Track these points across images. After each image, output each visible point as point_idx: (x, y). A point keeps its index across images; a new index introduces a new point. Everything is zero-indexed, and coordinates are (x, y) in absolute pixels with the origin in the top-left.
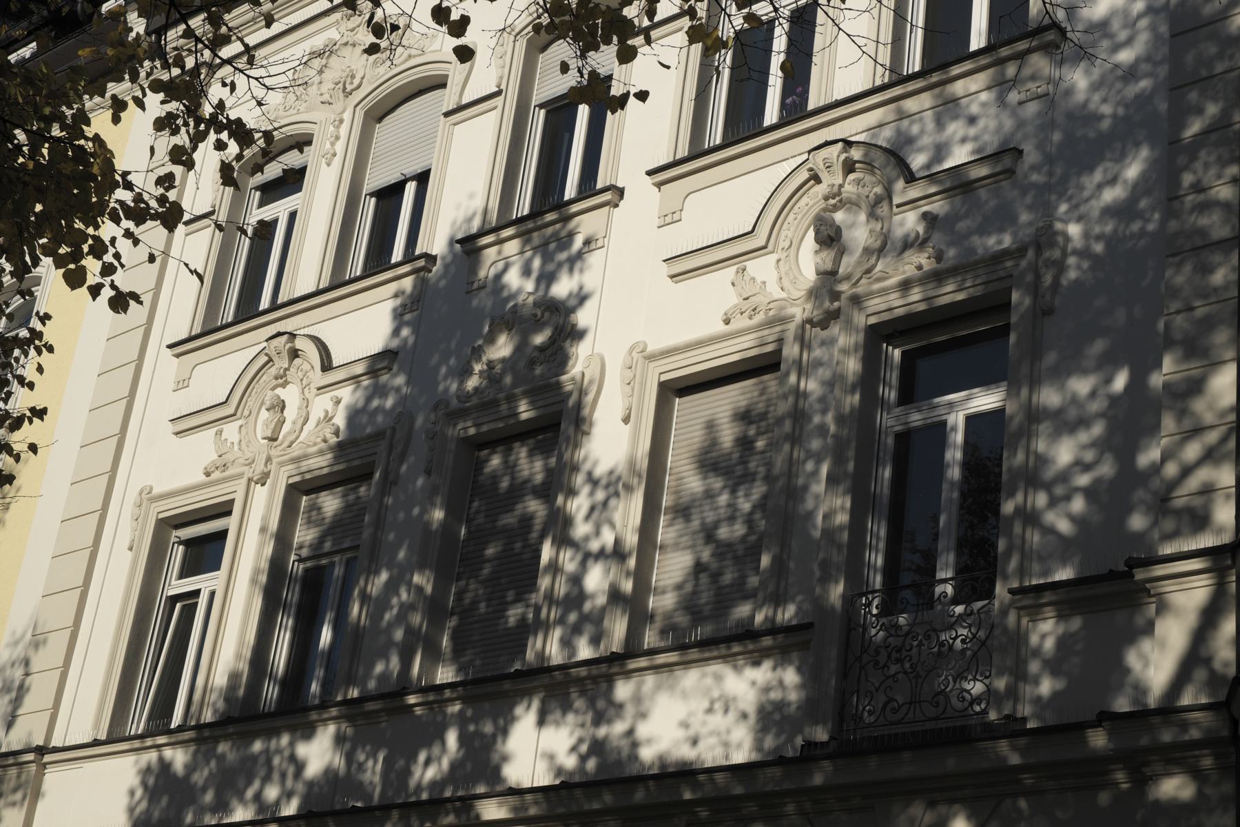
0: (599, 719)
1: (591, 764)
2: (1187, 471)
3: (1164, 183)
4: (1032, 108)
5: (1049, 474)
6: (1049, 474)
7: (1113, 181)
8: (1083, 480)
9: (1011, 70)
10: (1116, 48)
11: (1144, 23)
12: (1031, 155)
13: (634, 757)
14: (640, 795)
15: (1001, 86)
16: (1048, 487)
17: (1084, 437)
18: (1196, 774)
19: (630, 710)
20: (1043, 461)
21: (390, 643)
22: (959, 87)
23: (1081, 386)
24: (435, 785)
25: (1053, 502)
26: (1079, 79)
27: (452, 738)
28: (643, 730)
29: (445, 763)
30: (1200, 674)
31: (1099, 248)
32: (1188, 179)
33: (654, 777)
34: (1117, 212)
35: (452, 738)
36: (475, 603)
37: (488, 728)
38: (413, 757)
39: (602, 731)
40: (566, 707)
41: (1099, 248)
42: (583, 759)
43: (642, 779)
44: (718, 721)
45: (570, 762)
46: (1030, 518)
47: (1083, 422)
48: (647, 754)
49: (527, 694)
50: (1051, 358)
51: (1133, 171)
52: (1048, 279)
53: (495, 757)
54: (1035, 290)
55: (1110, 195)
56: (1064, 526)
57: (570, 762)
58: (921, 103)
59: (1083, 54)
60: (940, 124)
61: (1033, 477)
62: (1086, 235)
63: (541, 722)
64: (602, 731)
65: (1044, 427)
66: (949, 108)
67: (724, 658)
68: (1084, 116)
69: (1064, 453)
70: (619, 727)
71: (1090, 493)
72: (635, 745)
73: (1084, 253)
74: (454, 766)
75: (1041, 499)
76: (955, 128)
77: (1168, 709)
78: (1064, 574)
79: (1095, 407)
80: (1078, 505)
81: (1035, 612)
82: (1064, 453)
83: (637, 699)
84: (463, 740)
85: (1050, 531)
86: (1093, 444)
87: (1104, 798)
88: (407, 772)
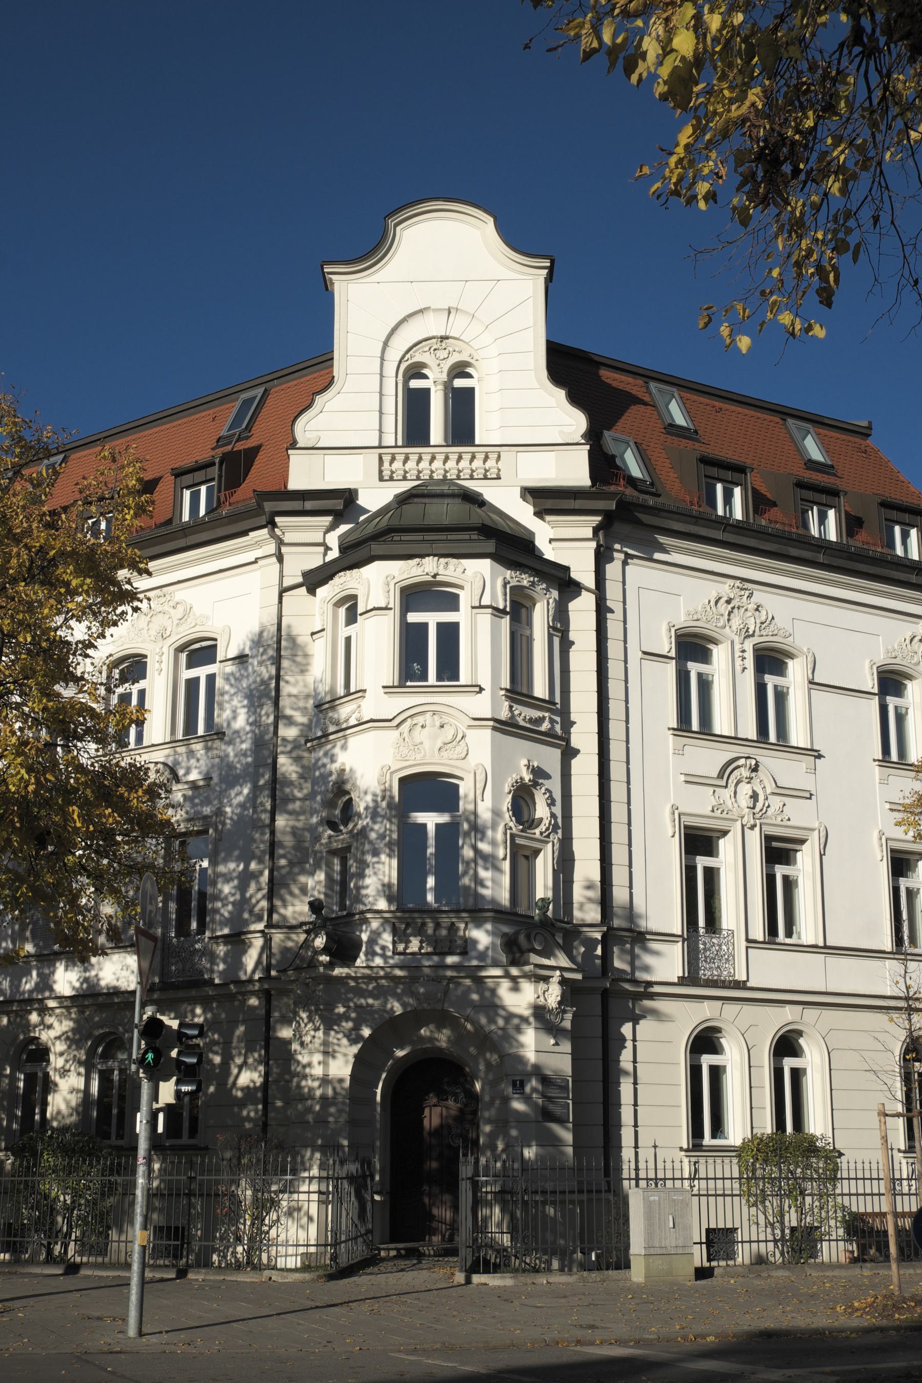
0: (86, 970)
1: (85, 986)
2: (258, 902)
3: (253, 798)
4: (217, 760)
5: (223, 896)
6: (223, 896)
7: (240, 793)
8: (231, 899)
9: (210, 743)
10: (242, 742)
11: (249, 735)
12: (216, 780)
13: (98, 984)
14: (101, 999)
15: (207, 749)
16: (222, 900)
17: (232, 884)
18: (259, 998)
19: (96, 967)
20: (221, 891)
21: (7, 935)
22: (194, 747)
23: (232, 866)
24: (31, 992)
25: (223, 906)
26: (230, 750)
27: (34, 973)
28: (101, 975)
29: (33, 983)
30: (260, 967)
31: (235, 818)
32: (259, 801)
33: (105, 994)
34: (242, 806)
35: (34, 973)
36: (38, 920)
37: (47, 971)
38: (20, 981)
39: (87, 974)
40: (74, 965)
41: (235, 818)
42: (82, 984)
43: (100, 994)
44: (125, 973)
45: (77, 985)
46: (216, 911)
47: (232, 879)
48: (103, 983)
49: (61, 960)
50: (223, 855)
51: (246, 791)
52: (220, 827)
53: (50, 982)
54: (216, 830)
55: (241, 799)
56: (226, 914)
57: (77, 985)
58: (182, 750)
59: (230, 743)
60: (188, 760)
61: (216, 897)
62: (233, 812)
63: (66, 969)
64: (87, 974)
65: (220, 880)
66: (191, 754)
67: (128, 952)
68: (231, 766)
69: (226, 889)
70: (93, 973)
71: (233, 903)
72: (99, 980)
73: (231, 819)
74: (37, 984)
75: (219, 904)
76: (193, 762)
77: (250, 981)
78: (226, 931)
79: (235, 874)
80: (230, 907)
81: (218, 944)
82: (226, 889)
83: (99, 963)
84: (38, 975)
85: (222, 915)
86: (235, 887)
87: (236, 1003)
88: (19, 986)
